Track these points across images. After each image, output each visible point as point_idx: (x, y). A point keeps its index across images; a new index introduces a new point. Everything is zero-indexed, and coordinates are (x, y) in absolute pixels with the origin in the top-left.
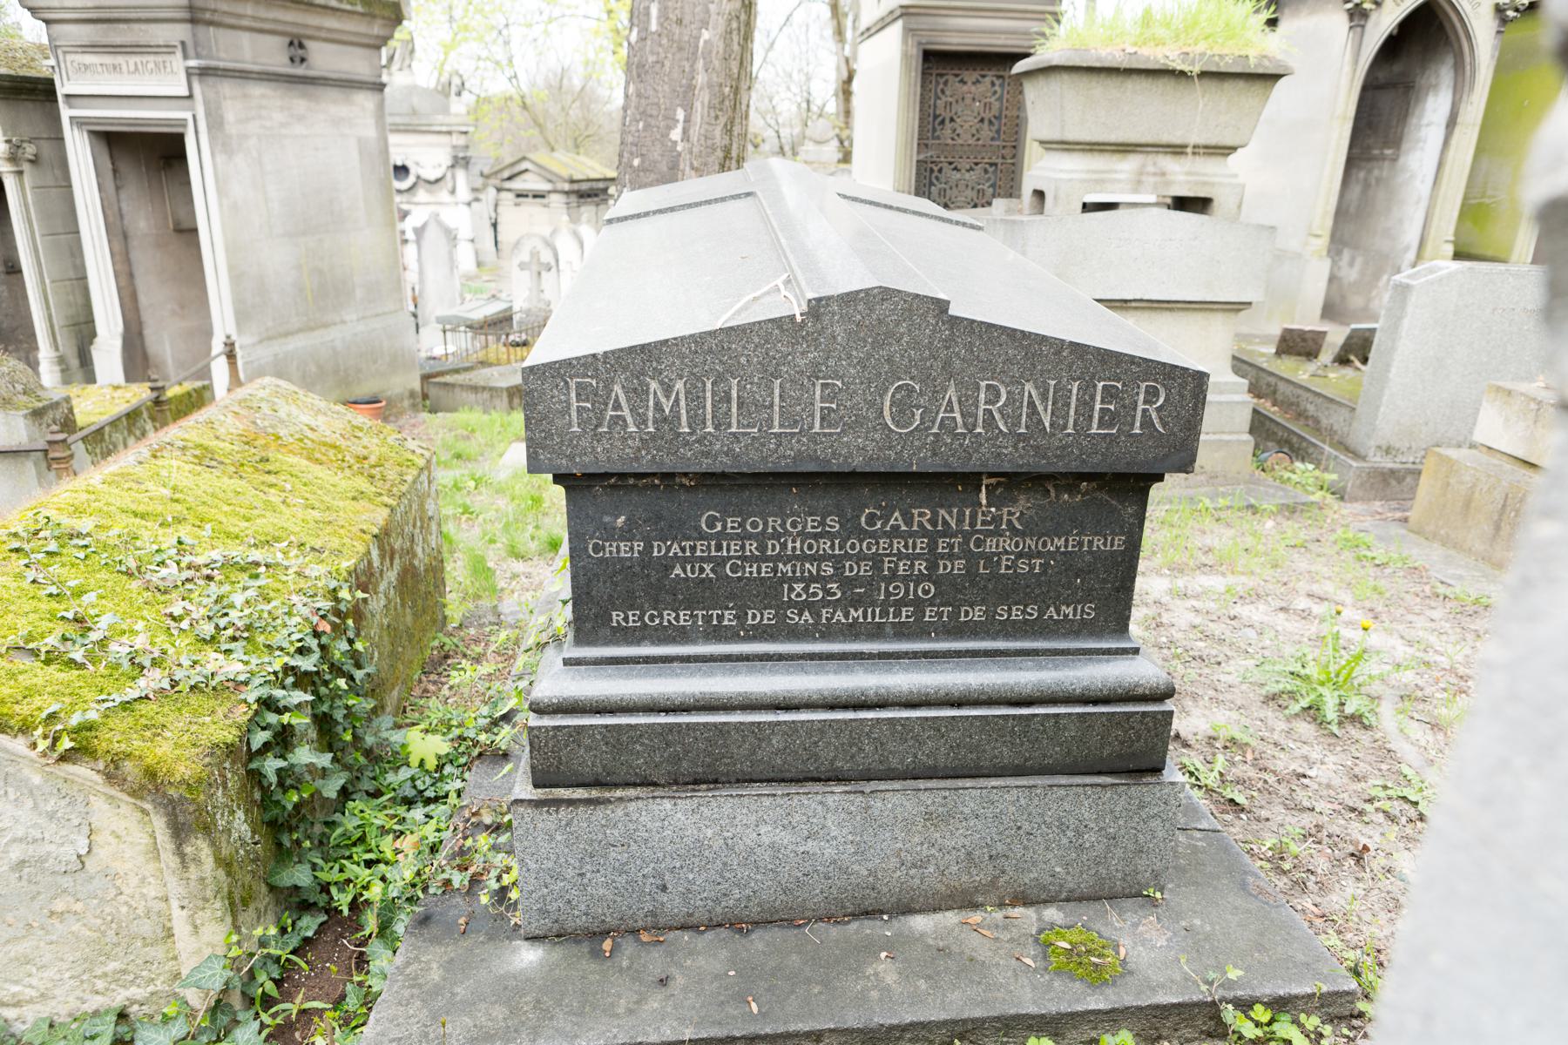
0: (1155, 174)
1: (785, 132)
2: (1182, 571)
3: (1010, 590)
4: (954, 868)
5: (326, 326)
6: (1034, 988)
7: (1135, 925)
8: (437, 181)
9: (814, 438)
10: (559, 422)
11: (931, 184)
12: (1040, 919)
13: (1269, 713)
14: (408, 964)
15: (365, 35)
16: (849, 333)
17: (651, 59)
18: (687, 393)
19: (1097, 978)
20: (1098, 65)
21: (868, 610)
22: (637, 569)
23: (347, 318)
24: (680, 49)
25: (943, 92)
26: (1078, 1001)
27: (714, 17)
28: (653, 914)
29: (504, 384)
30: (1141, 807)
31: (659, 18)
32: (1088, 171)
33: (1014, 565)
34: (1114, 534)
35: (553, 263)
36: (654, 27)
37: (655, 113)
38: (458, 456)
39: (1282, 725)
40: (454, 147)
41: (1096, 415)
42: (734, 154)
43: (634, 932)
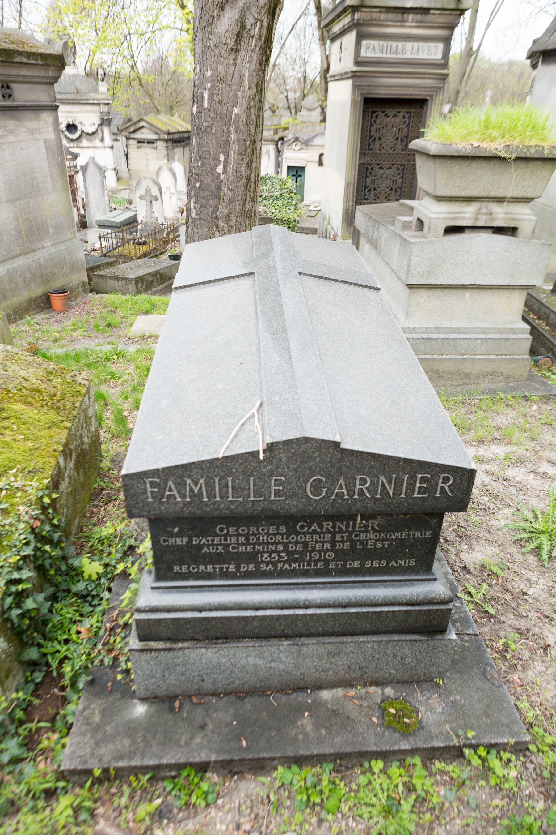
0: (486, 214)
1: (291, 95)
2: (483, 442)
3: (374, 554)
4: (342, 672)
5: (34, 251)
6: (376, 735)
7: (428, 699)
8: (93, 133)
9: (271, 502)
10: (142, 497)
11: (367, 177)
12: (383, 694)
13: (514, 550)
14: (84, 709)
15: (45, 77)
16: (288, 458)
17: (205, 124)
18: (206, 484)
19: (407, 732)
20: (456, 154)
21: (300, 567)
22: (185, 549)
23: (45, 245)
24: (221, 119)
25: (375, 122)
26: (396, 744)
27: (240, 99)
28: (199, 690)
29: (133, 276)
30: (434, 648)
31: (209, 100)
32: (448, 213)
33: (375, 544)
34: (426, 530)
35: (159, 196)
36: (206, 105)
37: (208, 156)
38: (109, 325)
39: (519, 558)
40: (102, 113)
41: (417, 489)
42: (253, 179)
43: (190, 697)
